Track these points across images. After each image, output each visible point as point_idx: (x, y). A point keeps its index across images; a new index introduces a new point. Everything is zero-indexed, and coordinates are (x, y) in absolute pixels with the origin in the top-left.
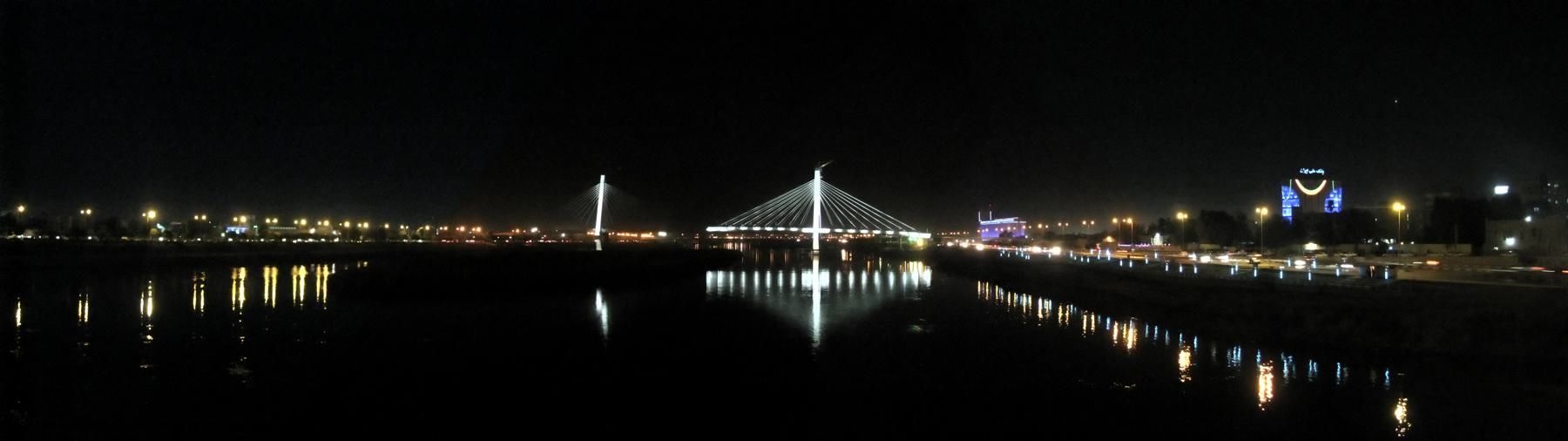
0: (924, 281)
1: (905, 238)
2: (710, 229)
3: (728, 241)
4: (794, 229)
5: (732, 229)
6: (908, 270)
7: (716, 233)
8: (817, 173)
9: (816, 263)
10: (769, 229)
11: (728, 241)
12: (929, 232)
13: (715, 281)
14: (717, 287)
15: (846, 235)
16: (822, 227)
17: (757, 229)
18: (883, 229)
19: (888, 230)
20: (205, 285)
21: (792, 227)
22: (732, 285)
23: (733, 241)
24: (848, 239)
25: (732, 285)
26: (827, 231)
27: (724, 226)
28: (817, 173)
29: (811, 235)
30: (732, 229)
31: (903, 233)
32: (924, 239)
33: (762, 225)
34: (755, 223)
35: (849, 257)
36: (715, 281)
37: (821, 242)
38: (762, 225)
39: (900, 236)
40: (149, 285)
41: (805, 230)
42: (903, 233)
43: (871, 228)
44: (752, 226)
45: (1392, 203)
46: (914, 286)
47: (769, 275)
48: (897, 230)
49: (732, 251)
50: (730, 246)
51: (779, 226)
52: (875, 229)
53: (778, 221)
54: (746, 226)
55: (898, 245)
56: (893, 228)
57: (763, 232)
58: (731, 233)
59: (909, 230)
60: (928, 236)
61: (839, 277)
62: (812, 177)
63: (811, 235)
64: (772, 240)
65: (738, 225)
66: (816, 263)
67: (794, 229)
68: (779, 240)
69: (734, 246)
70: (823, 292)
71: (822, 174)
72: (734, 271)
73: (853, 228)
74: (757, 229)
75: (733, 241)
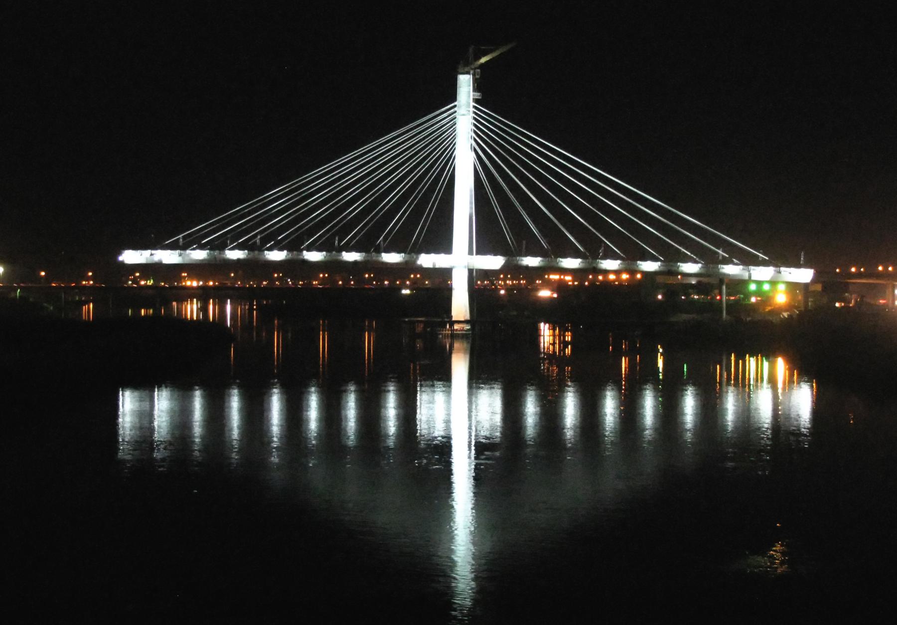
0: (788, 417)
1: (738, 285)
2: (130, 257)
3: (190, 294)
4: (392, 258)
5: (199, 255)
6: (742, 383)
7: (148, 269)
8: (465, 84)
9: (460, 367)
10: (314, 257)
11: (190, 294)
12: (807, 265)
13: (146, 416)
14: (152, 430)
15: (554, 277)
16: (481, 251)
17: (277, 256)
18: (672, 257)
19: (686, 259)
20: (253, 308)
21: (388, 250)
22: (197, 429)
23: (203, 295)
24: (560, 287)
25: (197, 429)
26: (495, 262)
27: (173, 247)
28: (465, 84)
29: (446, 274)
30: (199, 255)
31: (731, 270)
32: (793, 287)
33: (294, 245)
34: (272, 240)
35: (565, 344)
36: (146, 416)
37: (475, 294)
38: (294, 245)
39: (722, 279)
40: (198, 281)
41: (426, 260)
42: (731, 270)
43: (633, 254)
44: (261, 248)
45: (748, 290)
46: (797, 433)
47: (235, 403)
48: (710, 259)
49: (201, 325)
50: (192, 309)
51: (349, 249)
52: (646, 257)
53: (310, 233)
54: (240, 247)
55: (715, 308)
56: (702, 255)
57: (334, 266)
58: (194, 269)
59: (749, 261)
60: (805, 275)
61: (531, 408)
62: (451, 96)
63: (446, 274)
64: (329, 293)
65: (219, 245)
66: (460, 367)
67: (392, 258)
68: (345, 290)
69: (204, 309)
70: (481, 448)
71: (478, 86)
72: (204, 386)
73: (576, 254)
74: (277, 256)
75: (203, 295)
